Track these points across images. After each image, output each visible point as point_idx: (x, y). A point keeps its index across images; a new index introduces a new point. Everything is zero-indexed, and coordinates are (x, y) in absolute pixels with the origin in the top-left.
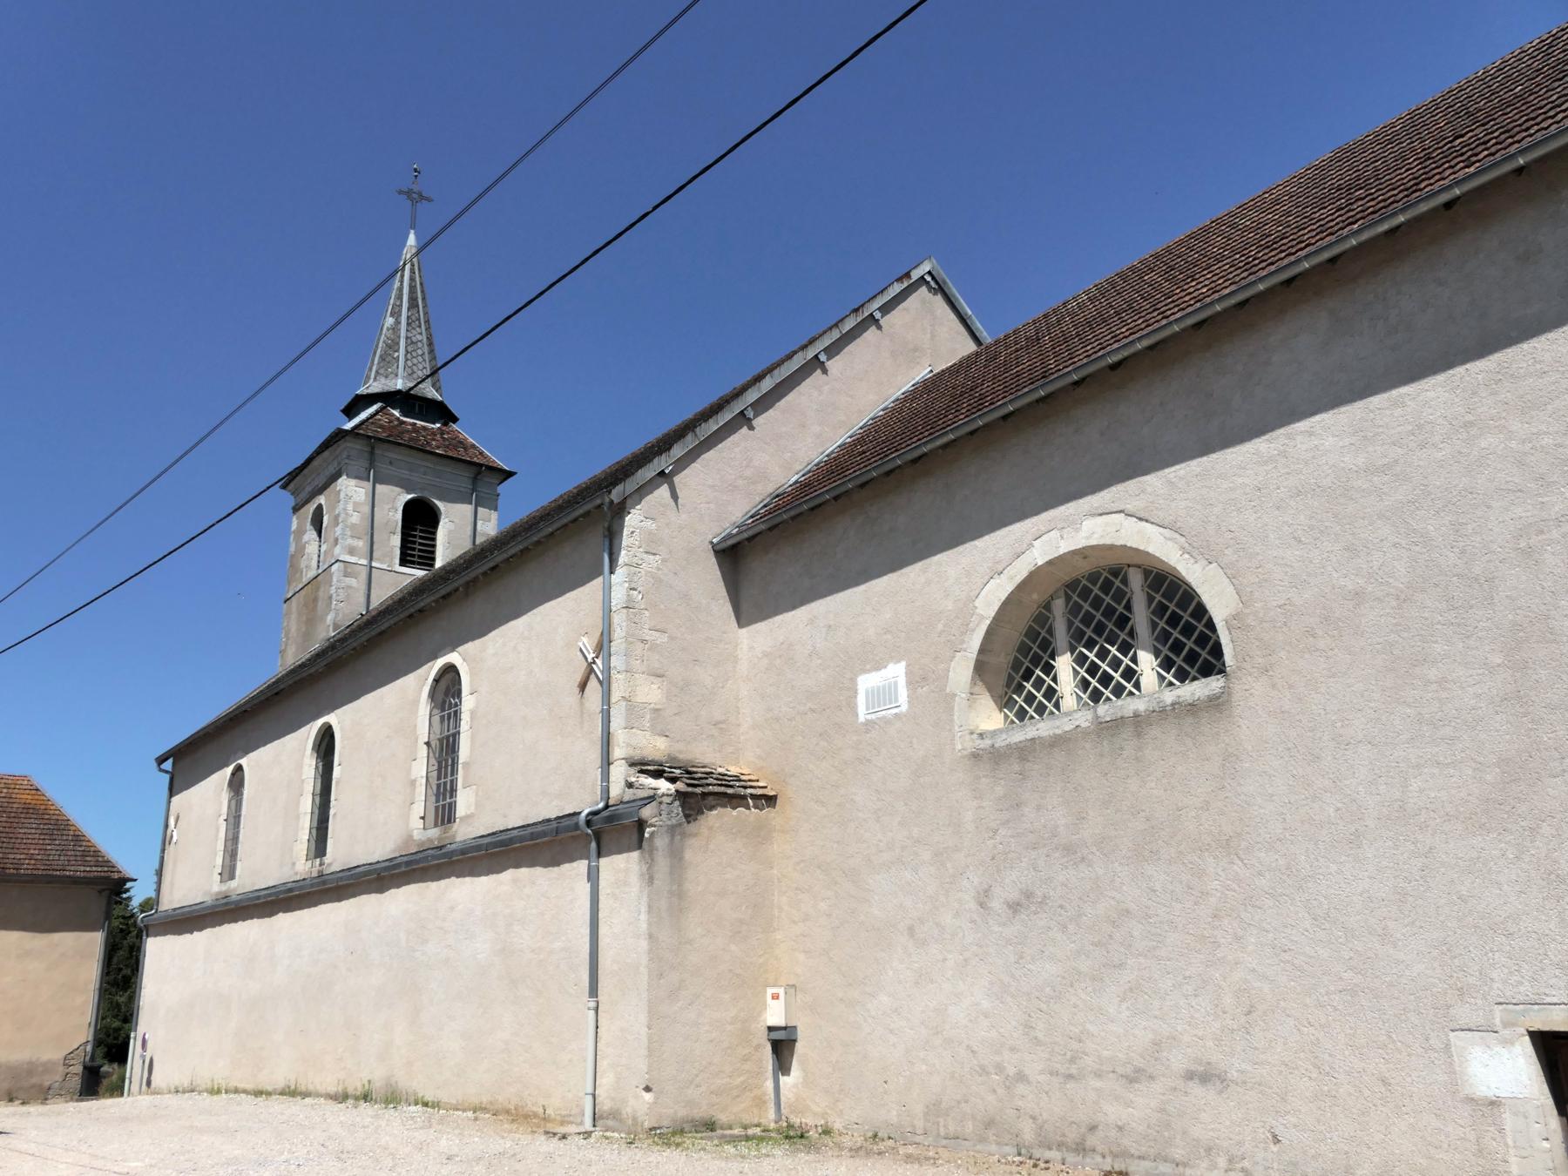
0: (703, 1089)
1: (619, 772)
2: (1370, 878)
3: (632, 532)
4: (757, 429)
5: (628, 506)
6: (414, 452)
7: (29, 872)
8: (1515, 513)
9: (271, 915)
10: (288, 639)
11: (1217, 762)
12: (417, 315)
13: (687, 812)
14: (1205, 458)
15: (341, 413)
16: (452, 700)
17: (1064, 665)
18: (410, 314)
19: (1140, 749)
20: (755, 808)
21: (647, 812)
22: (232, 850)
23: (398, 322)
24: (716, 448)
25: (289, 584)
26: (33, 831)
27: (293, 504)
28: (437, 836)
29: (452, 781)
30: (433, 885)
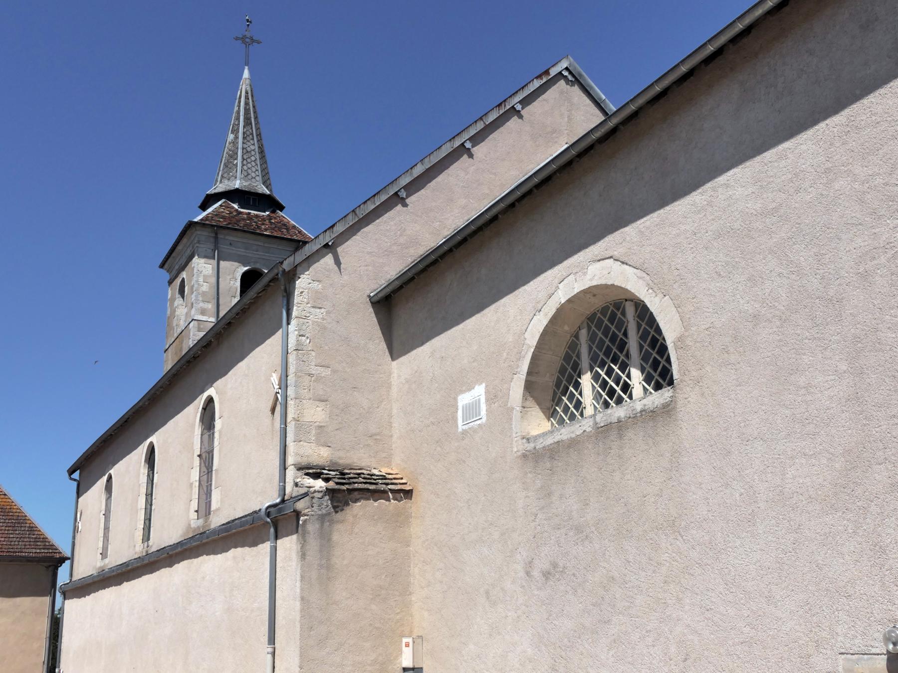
1: (291, 473)
2: (761, 550)
3: (302, 293)
5: (298, 272)
6: (248, 235)
8: (857, 244)
9: (120, 584)
11: (668, 457)
12: (250, 131)
13: (335, 504)
14: (662, 211)
17: (586, 380)
18: (245, 130)
19: (621, 448)
23: (236, 138)
24: (373, 223)
25: (167, 337)
27: (168, 278)
28: (202, 524)
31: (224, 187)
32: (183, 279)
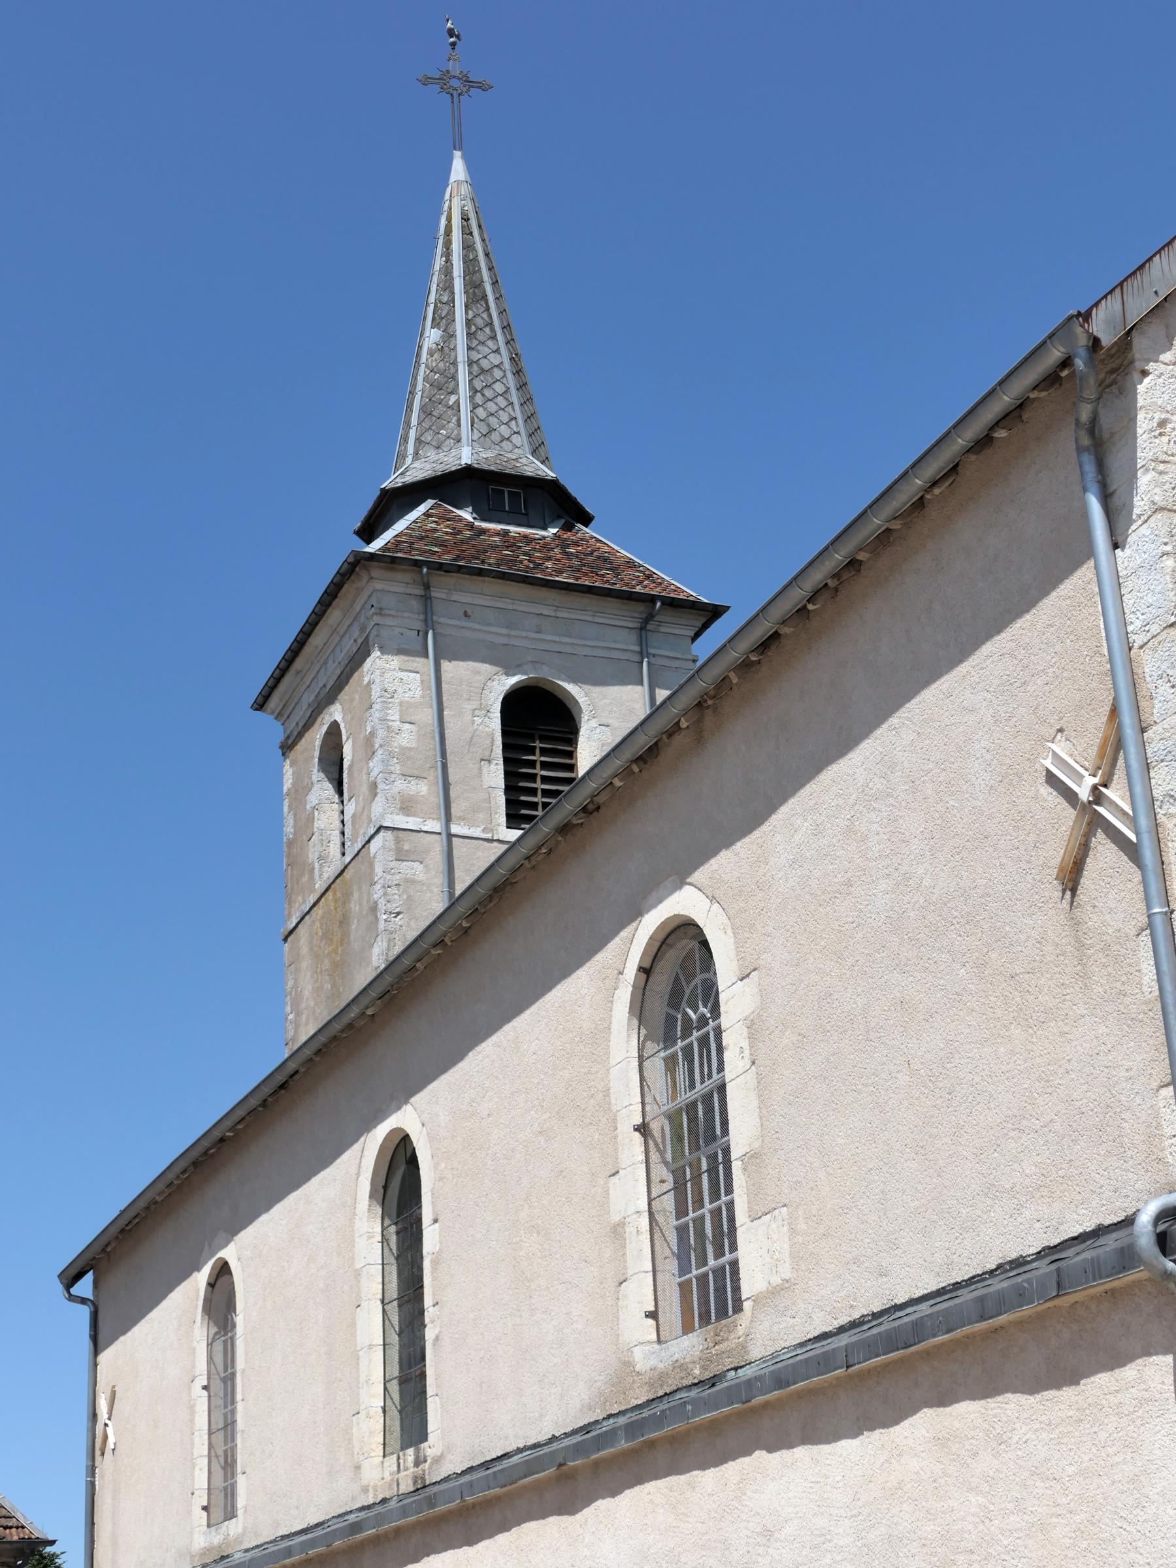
3: (1162, 424)
10: (298, 1014)
12: (485, 316)
16: (690, 1012)
22: (226, 1452)
23: (449, 336)
27: (281, 737)
29: (717, 1213)
30: (707, 1479)
31: (428, 466)
32: (335, 726)
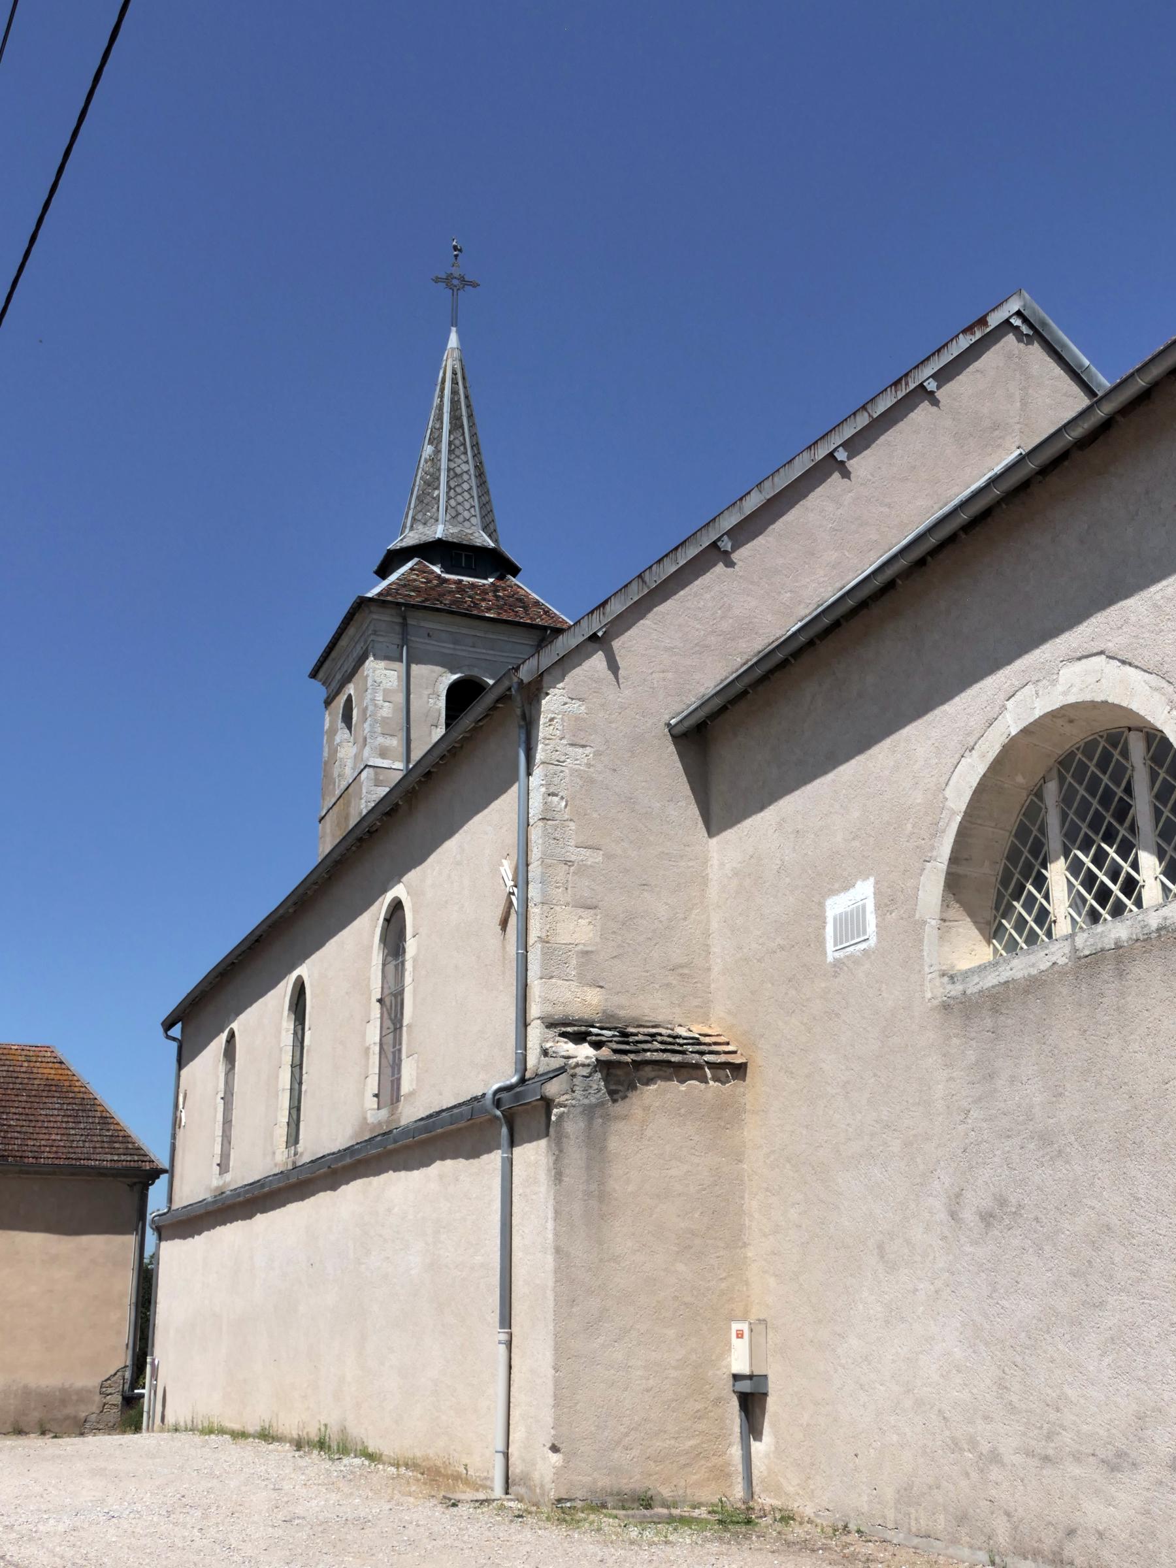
0: (635, 1452)
1: (536, 1032)
3: (552, 720)
4: (739, 564)
5: (545, 686)
6: (458, 619)
7: (50, 1161)
9: (250, 1216)
12: (461, 438)
13: (613, 1087)
15: (375, 576)
17: (1057, 873)
18: (452, 437)
19: (1122, 994)
20: (715, 1081)
21: (552, 1089)
23: (438, 451)
26: (56, 1112)
27: (325, 696)
31: (417, 537)
